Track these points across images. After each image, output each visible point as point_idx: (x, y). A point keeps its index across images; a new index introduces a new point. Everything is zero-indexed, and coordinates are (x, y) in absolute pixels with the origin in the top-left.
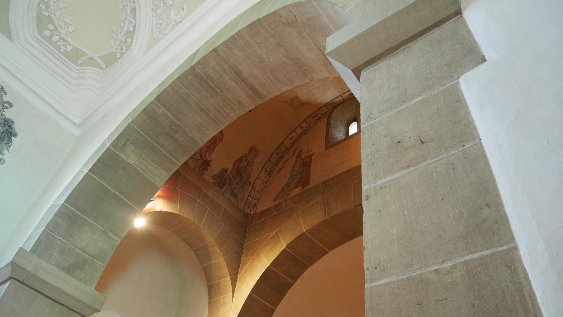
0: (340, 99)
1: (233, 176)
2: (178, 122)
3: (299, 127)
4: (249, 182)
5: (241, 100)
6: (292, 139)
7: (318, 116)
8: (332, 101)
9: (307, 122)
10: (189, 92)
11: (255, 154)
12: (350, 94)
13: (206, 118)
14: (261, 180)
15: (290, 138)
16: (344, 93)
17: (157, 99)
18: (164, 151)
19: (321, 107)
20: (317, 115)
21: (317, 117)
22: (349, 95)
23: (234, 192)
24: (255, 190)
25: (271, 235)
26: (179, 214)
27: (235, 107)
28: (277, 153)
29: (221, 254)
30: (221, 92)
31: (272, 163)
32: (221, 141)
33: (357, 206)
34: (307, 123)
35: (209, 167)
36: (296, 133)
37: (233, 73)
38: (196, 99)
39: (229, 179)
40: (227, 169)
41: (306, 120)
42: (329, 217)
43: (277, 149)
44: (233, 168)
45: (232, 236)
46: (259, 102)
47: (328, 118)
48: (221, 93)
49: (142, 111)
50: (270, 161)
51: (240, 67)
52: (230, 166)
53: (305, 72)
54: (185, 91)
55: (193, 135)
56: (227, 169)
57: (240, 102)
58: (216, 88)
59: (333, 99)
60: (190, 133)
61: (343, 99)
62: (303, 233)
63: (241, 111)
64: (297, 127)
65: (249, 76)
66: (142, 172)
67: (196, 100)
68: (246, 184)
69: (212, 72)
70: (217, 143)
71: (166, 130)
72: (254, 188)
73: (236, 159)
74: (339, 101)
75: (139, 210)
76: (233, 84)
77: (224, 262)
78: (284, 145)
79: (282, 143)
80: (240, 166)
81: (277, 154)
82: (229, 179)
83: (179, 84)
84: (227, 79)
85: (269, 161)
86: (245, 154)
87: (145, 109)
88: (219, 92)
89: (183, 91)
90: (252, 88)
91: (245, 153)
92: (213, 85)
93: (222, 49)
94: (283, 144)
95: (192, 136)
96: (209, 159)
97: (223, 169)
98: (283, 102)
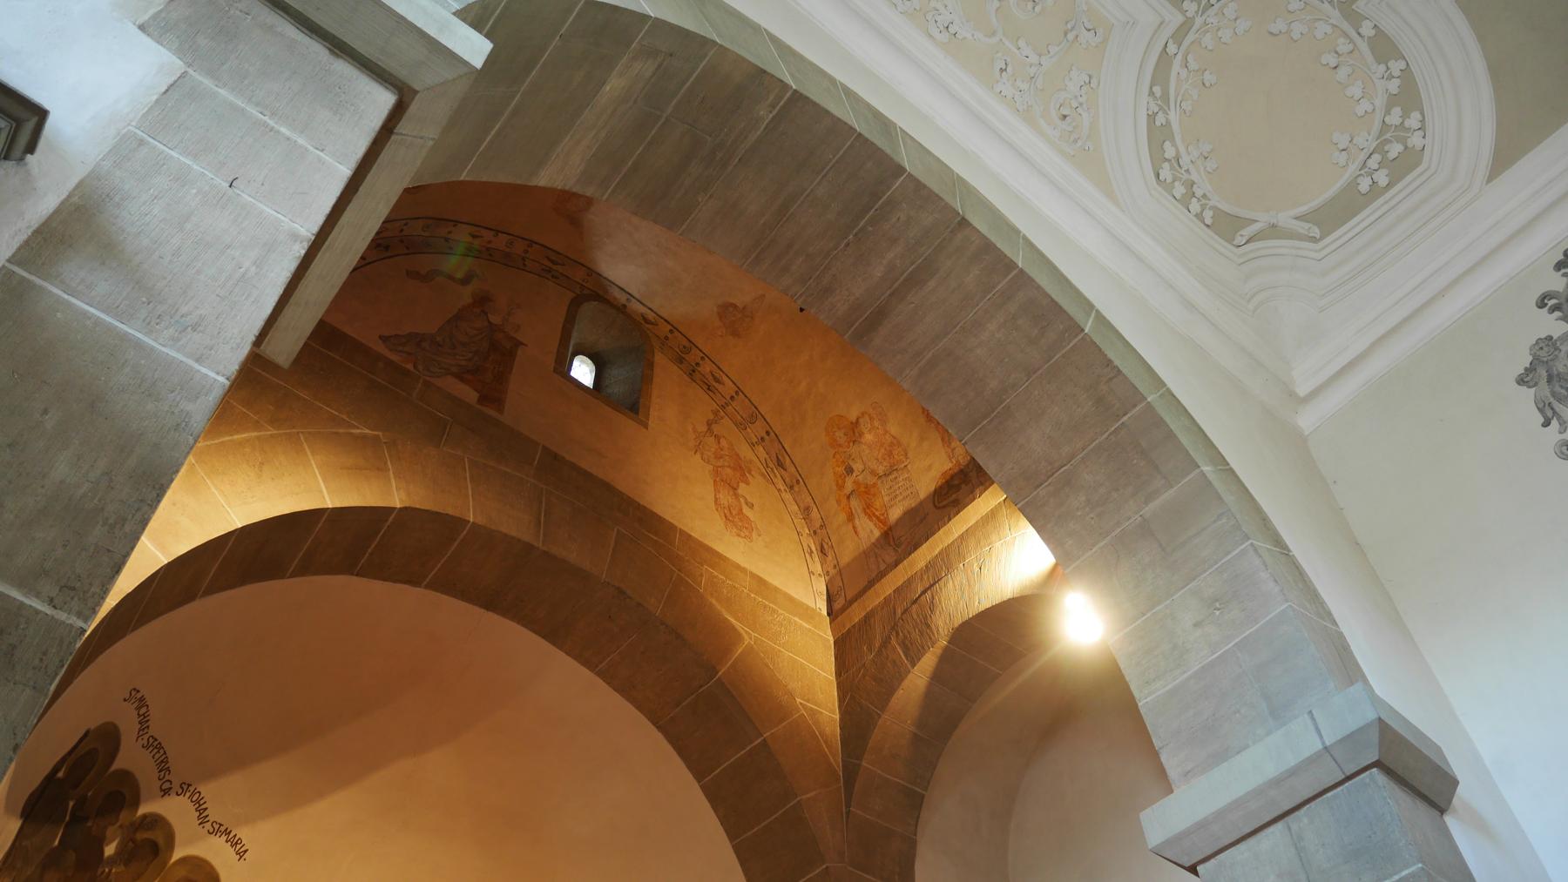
0: (622, 298)
2: (737, 160)
7: (555, 267)
8: (609, 283)
9: (529, 249)
10: (831, 168)
13: (762, 222)
16: (643, 301)
17: (798, 98)
19: (582, 265)
20: (557, 264)
21: (550, 265)
25: (359, 431)
27: (811, 281)
30: (847, 245)
31: (402, 231)
37: (911, 269)
38: (812, 190)
41: (534, 245)
49: (756, 66)
51: (932, 284)
54: (831, 160)
55: (701, 204)
58: (855, 231)
59: (614, 284)
61: (624, 306)
62: (464, 520)
67: (809, 190)
69: (899, 219)
71: (708, 137)
74: (615, 299)
75: (1133, 626)
76: (878, 272)
83: (849, 143)
84: (890, 255)
85: (404, 222)
87: (765, 72)
89: (831, 157)
90: (880, 315)
92: (862, 223)
93: (973, 239)
94: (455, 226)
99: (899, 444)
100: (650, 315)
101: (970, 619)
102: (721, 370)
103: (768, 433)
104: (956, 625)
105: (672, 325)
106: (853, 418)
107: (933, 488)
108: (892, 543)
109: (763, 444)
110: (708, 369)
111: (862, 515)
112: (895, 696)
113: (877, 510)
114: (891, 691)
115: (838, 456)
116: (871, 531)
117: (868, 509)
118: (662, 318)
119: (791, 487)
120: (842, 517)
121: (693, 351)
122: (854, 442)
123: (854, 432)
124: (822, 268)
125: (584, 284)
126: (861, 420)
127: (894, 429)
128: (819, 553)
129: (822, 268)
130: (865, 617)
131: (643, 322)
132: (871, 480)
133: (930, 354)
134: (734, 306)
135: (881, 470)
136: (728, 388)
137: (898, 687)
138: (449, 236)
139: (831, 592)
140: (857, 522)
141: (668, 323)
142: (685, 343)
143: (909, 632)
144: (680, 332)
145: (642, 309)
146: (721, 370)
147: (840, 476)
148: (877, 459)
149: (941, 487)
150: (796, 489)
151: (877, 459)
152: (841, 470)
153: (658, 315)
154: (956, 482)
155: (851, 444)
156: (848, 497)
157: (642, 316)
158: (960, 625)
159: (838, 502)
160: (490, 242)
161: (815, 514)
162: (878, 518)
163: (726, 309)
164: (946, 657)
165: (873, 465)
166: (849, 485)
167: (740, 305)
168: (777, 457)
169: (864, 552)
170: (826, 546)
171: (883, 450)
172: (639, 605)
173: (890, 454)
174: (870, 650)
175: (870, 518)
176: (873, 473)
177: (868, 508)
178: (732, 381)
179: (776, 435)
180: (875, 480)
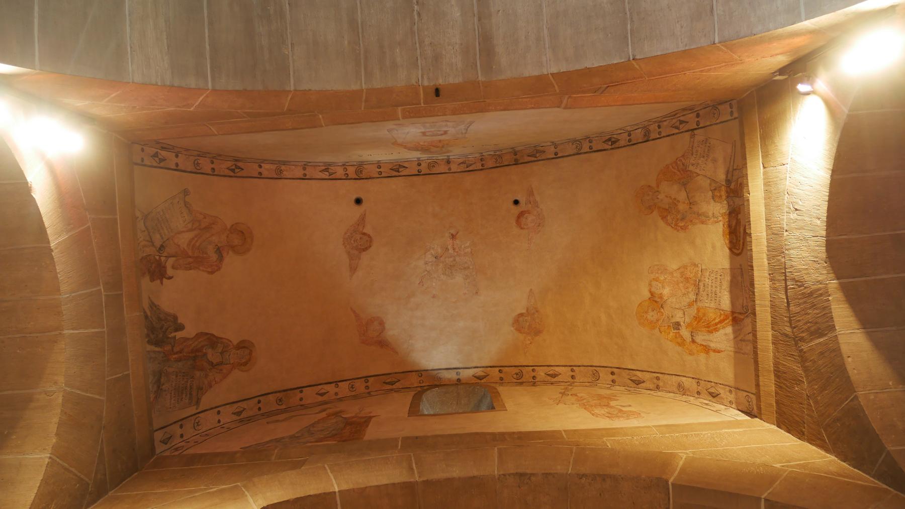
0: (452, 375)
1: (180, 352)
2: (287, 5)
3: (349, 382)
4: (198, 399)
5: (444, 53)
6: (322, 395)
11: (244, 361)
12: (476, 375)
13: (346, 42)
14: (219, 421)
15: (320, 392)
18: (206, 31)
22: (473, 376)
23: (162, 380)
24: (196, 425)
26: (52, 250)
28: (280, 400)
29: (54, 440)
30: (419, 14)
31: (260, 409)
32: (209, 273)
33: (509, 475)
34: (367, 388)
35: (159, 281)
36: (337, 390)
39: (173, 347)
40: (180, 328)
42: (421, 480)
43: (284, 391)
44: (192, 339)
45: (102, 441)
46: (480, 75)
47: (415, 394)
48: (416, 17)
50: (259, 402)
52: (189, 331)
53: (629, 35)
56: (180, 328)
57: (437, 58)
60: (290, 46)
61: (459, 380)
62: (330, 493)
63: (425, 77)
64: (346, 380)
65: (499, 11)
66: (127, 13)
68: (191, 394)
70: (201, 268)
72: (197, 421)
73: (207, 332)
74: (449, 380)
77: (44, 469)
78: (300, 395)
79: (300, 389)
80: (204, 351)
81: (278, 401)
82: (173, 347)
85: (257, 399)
86: (230, 343)
88: (416, 11)
91: (231, 341)
94: (301, 392)
95: (288, 55)
96: (170, 272)
97: (175, 318)
98: (354, 312)
99: (685, 267)
100: (479, 372)
101: (827, 236)
102: (552, 366)
103: (613, 373)
104: (824, 255)
105: (498, 367)
106: (647, 295)
107: (728, 251)
108: (742, 317)
109: (616, 384)
110: (543, 374)
111: (711, 337)
112: (849, 368)
113: (714, 319)
114: (841, 368)
115: (662, 329)
116: (726, 334)
117: (711, 328)
118: (487, 367)
119: (658, 387)
120: (702, 357)
121: (524, 372)
122: (662, 306)
123: (656, 302)
124: (418, 45)
125: (422, 385)
126: (653, 290)
127: (673, 265)
128: (714, 400)
129: (418, 45)
130: (776, 375)
131: (479, 381)
132: (693, 311)
133: (546, 31)
134: (521, 315)
135: (692, 297)
136: (565, 372)
137: (843, 359)
138: (302, 403)
139: (745, 409)
140: (713, 345)
141: (493, 367)
142: (516, 370)
143: (806, 323)
144: (506, 366)
145: (471, 372)
146: (552, 366)
147: (676, 337)
148: (685, 294)
149: (731, 242)
150: (661, 384)
151: (685, 294)
152: (672, 332)
153: (483, 367)
154: (734, 223)
155: (662, 310)
156: (693, 341)
157: (475, 377)
158: (827, 251)
159: (691, 354)
160: (336, 394)
161: (687, 382)
162: (720, 322)
163: (518, 322)
164: (852, 296)
165: (686, 301)
166: (685, 333)
167: (524, 311)
168: (631, 380)
169: (736, 352)
170: (712, 390)
171: (681, 285)
172: (546, 475)
173: (687, 279)
174: (799, 382)
175: (716, 330)
176: (690, 305)
177: (709, 327)
178: (562, 366)
179: (617, 368)
180: (695, 307)
